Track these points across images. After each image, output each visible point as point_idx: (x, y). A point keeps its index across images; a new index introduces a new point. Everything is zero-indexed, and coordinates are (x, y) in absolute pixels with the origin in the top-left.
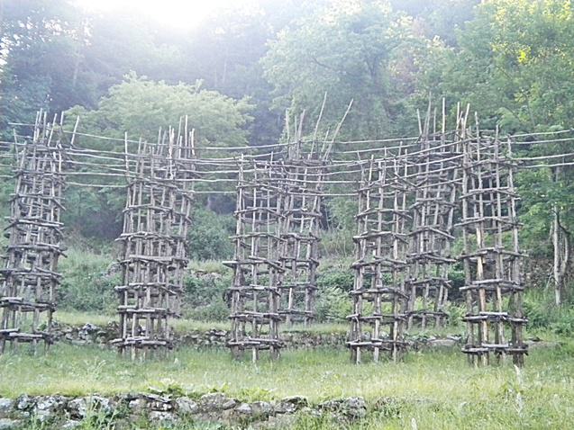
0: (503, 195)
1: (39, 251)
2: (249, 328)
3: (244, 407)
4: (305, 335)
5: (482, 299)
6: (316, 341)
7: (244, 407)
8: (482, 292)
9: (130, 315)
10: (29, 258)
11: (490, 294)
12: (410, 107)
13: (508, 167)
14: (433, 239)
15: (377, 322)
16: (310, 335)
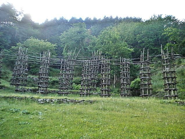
0: (108, 69)
1: (24, 75)
2: (62, 90)
3: (76, 101)
4: (71, 92)
5: (104, 87)
6: (73, 93)
7: (76, 101)
8: (104, 85)
9: (40, 87)
10: (22, 76)
11: (105, 85)
12: (89, 48)
13: (109, 64)
14: (94, 75)
15: (85, 90)
16: (72, 92)
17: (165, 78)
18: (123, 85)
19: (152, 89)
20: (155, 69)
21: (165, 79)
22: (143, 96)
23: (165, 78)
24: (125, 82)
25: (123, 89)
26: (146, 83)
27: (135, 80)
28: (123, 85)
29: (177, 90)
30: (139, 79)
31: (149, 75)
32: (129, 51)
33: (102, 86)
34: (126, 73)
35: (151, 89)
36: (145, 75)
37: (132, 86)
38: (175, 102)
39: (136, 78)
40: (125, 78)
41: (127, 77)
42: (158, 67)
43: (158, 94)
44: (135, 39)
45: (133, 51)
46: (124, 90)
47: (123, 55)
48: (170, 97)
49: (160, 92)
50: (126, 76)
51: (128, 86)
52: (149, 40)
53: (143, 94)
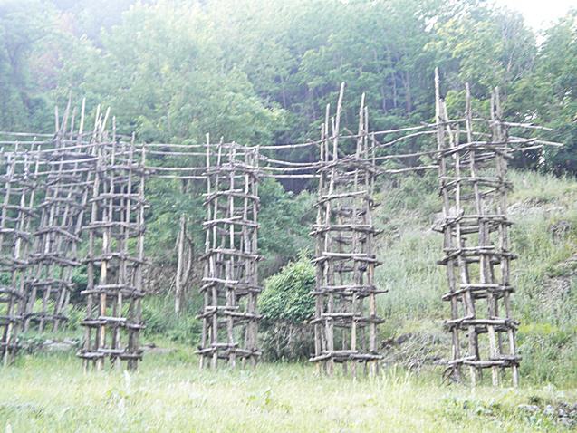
8: (103, 297)
12: (50, 103)
13: (141, 174)
14: (59, 241)
17: (455, 257)
18: (214, 299)
19: (377, 321)
20: (386, 220)
21: (450, 263)
22: (327, 359)
23: (455, 257)
24: (227, 281)
25: (215, 320)
26: (350, 286)
27: (288, 271)
28: (214, 299)
29: (514, 329)
30: (251, 328)
31: (363, 241)
32: (261, 117)
33: (90, 302)
34: (237, 228)
35: (376, 323)
36: (340, 241)
37: (269, 301)
38: (529, 407)
39: (293, 258)
40: (226, 257)
41: (240, 253)
42: (404, 211)
43: (404, 346)
44: (294, 70)
45: (279, 119)
46: (219, 328)
47: (224, 131)
48: (479, 368)
49: (418, 338)
50: (237, 245)
51: (245, 301)
52: (361, 77)
53: (331, 352)
